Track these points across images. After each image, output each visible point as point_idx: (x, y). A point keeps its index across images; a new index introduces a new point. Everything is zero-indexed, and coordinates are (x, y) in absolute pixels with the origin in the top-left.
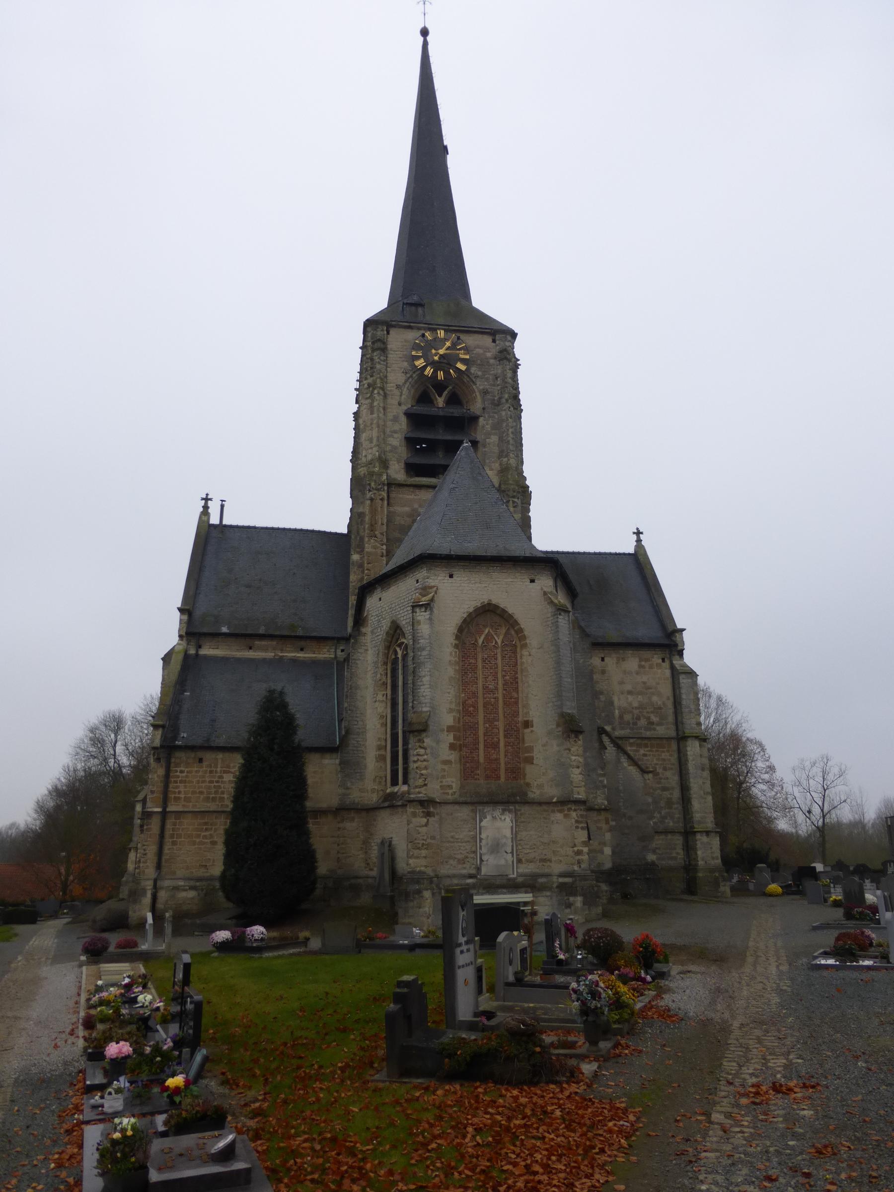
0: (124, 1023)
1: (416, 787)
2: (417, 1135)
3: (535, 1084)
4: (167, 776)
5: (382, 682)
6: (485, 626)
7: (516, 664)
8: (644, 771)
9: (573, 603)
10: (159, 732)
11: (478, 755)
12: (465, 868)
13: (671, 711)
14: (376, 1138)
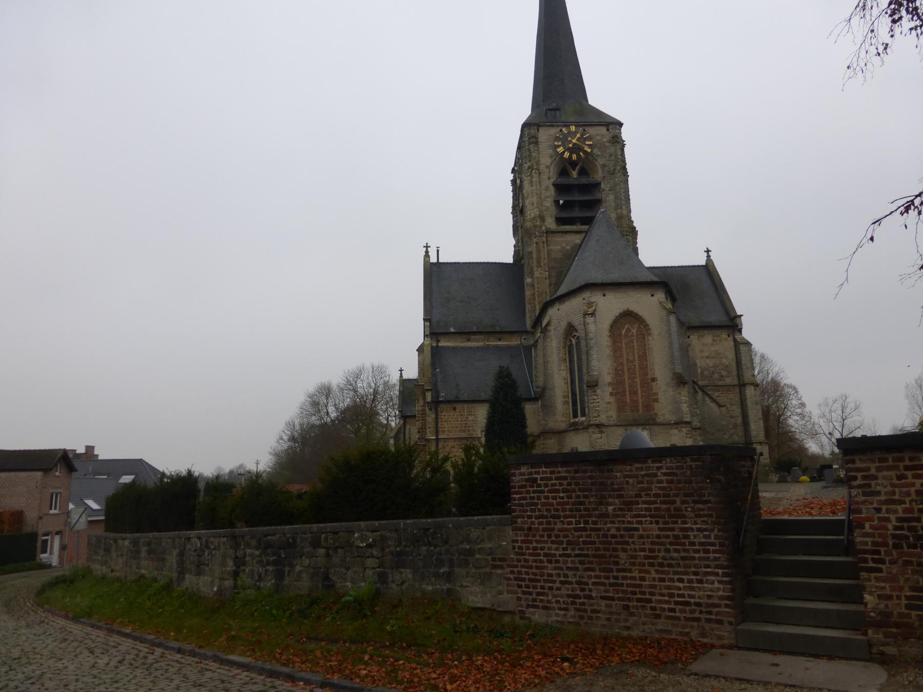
1: (594, 417)
4: (437, 418)
6: (626, 324)
7: (645, 344)
8: (720, 406)
13: (734, 368)
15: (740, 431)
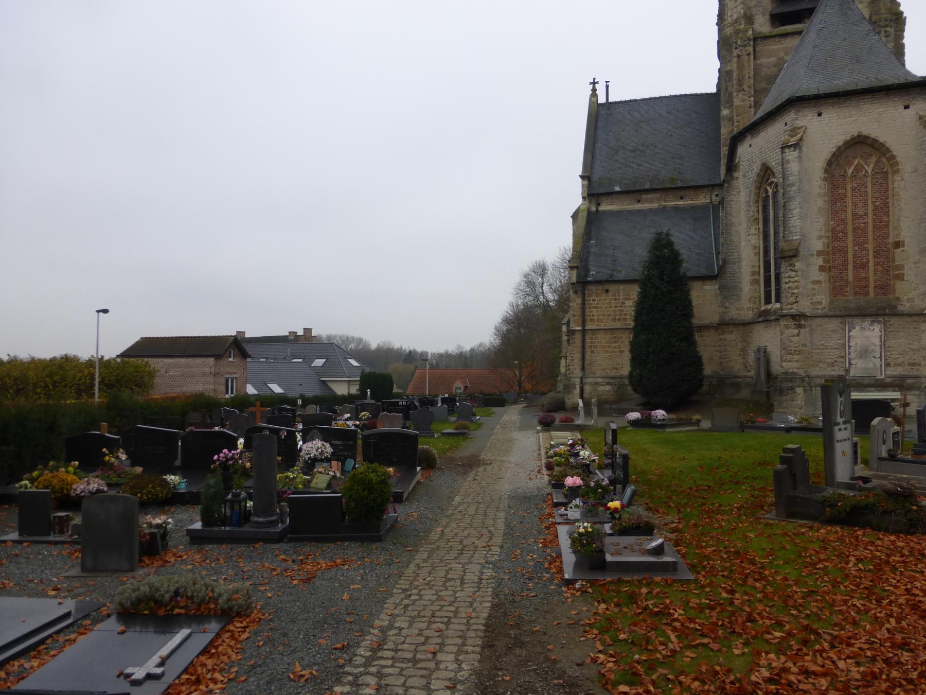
0: (573, 467)
1: (788, 304)
2: (806, 557)
3: (912, 534)
4: (583, 303)
5: (754, 218)
6: (855, 158)
7: (887, 190)
10: (575, 272)
11: (848, 275)
14: (771, 556)
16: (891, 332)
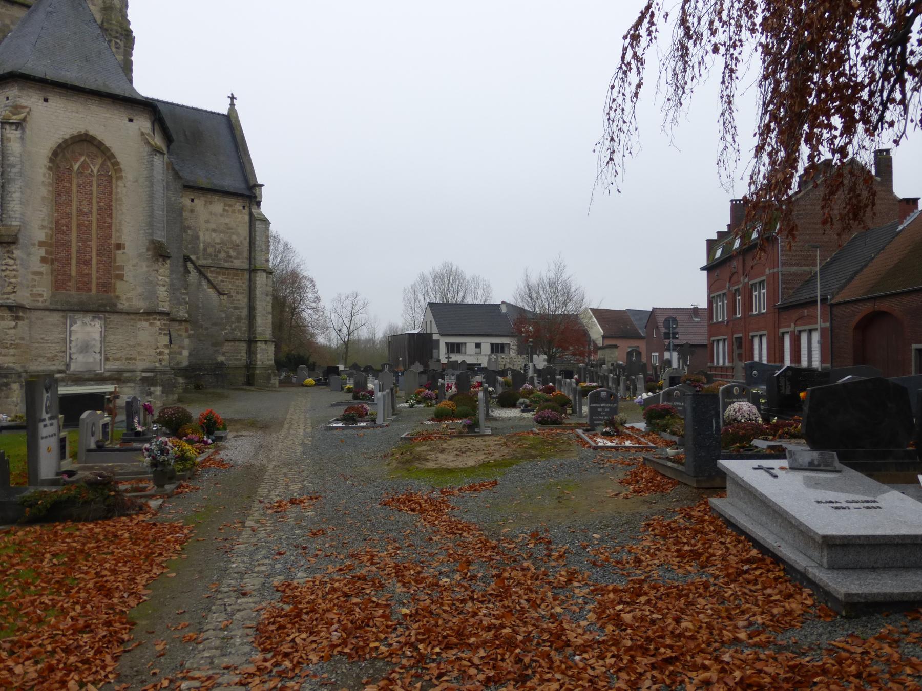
6: (81, 154)
7: (111, 193)
8: (220, 293)
9: (168, 147)
12: (54, 365)
15: (244, 325)
16: (111, 328)
